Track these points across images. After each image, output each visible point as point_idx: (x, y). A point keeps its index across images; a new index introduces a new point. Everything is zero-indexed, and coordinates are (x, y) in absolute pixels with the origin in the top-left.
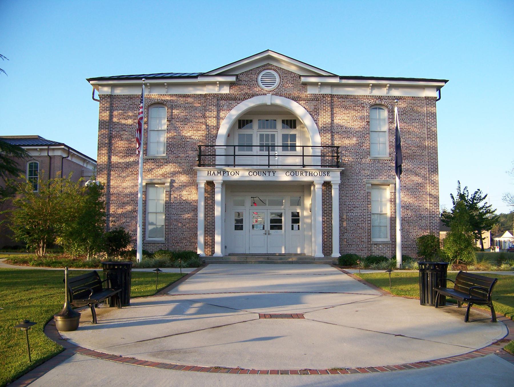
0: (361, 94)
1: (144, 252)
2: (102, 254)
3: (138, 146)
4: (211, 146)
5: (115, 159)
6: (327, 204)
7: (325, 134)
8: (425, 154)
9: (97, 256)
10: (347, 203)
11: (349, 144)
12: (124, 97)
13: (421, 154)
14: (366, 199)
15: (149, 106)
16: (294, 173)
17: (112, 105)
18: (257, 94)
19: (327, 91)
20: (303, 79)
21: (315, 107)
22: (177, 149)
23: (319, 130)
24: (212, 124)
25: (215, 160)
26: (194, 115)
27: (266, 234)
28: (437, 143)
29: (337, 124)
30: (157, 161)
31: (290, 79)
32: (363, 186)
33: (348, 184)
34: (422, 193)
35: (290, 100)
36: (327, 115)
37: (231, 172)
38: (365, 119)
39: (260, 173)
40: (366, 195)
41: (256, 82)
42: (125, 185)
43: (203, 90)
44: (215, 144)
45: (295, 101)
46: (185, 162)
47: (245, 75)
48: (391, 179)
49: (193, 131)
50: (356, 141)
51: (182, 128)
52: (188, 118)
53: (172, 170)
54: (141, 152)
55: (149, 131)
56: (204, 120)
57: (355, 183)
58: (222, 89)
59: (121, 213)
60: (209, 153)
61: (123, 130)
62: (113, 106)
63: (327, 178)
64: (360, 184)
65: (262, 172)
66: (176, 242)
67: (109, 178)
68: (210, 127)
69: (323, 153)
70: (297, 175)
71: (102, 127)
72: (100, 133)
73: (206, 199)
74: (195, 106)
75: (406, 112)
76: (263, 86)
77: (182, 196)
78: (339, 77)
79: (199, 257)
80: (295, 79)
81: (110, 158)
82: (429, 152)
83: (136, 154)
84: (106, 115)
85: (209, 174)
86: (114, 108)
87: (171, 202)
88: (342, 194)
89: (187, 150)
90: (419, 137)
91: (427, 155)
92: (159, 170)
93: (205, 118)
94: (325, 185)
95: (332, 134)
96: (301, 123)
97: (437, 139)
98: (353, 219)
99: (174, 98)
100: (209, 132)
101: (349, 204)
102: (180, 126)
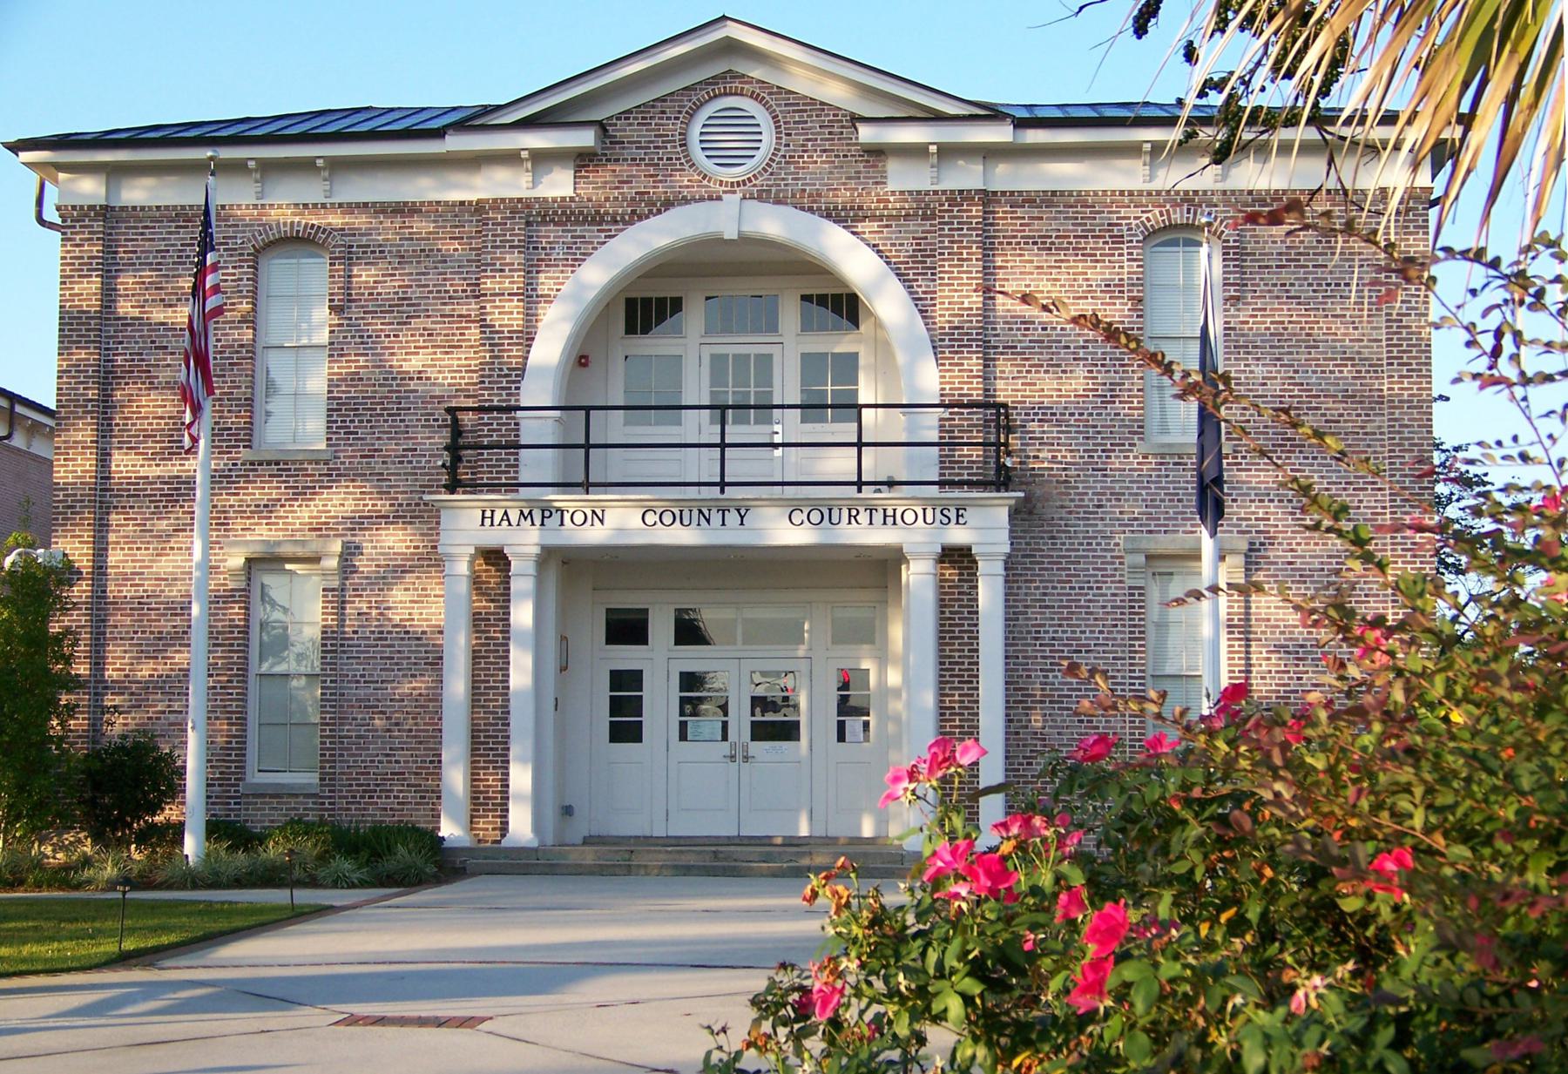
0: (1109, 186)
1: (214, 829)
2: (69, 837)
3: (188, 418)
4: (499, 409)
5: (124, 464)
6: (963, 638)
7: (957, 352)
8: (1380, 427)
9: (50, 848)
10: (1047, 632)
11: (1055, 393)
12: (158, 214)
13: (1363, 428)
14: (1127, 617)
15: (258, 252)
16: (826, 513)
17: (111, 246)
18: (684, 198)
19: (967, 176)
20: (866, 134)
21: (919, 244)
22: (368, 421)
23: (931, 336)
24: (506, 322)
25: (517, 466)
26: (434, 286)
27: (733, 758)
28: (1430, 383)
29: (1008, 311)
30: (290, 470)
31: (819, 133)
32: (1113, 563)
33: (1052, 557)
34: (1361, 589)
35: (816, 218)
36: (964, 276)
37: (571, 511)
38: (1126, 289)
39: (686, 514)
40: (1127, 598)
41: (679, 149)
42: (165, 565)
43: (471, 188)
44: (517, 400)
45: (838, 220)
46: (399, 474)
47: (635, 118)
48: (1231, 532)
49: (430, 350)
50: (1085, 378)
51: (389, 336)
52: (410, 299)
53: (350, 506)
54: (202, 443)
55: (259, 350)
56: (473, 306)
57: (1078, 550)
58: (546, 179)
59: (150, 676)
60: (495, 438)
61: (156, 348)
62: (116, 252)
63: (958, 536)
64: (1099, 554)
65: (695, 512)
66: (364, 791)
67: (103, 537)
68: (497, 332)
69: (948, 432)
70: (835, 520)
71: (71, 336)
72: (64, 360)
73: (478, 621)
74: (439, 250)
75: (1300, 254)
76: (708, 165)
77: (389, 608)
78: (1009, 120)
79: (440, 849)
80: (836, 130)
81: (104, 458)
82: (1396, 420)
83: (183, 447)
84: (90, 287)
85: (488, 522)
86: (121, 258)
87: (344, 633)
88: (1026, 594)
89: (407, 426)
90: (1353, 359)
91: (1386, 430)
92: (300, 506)
93: (478, 297)
94: (955, 562)
95: (985, 354)
96: (870, 314)
97: (1430, 364)
98: (1071, 696)
99: (360, 221)
100: (493, 351)
101: (1054, 639)
102: (381, 330)
